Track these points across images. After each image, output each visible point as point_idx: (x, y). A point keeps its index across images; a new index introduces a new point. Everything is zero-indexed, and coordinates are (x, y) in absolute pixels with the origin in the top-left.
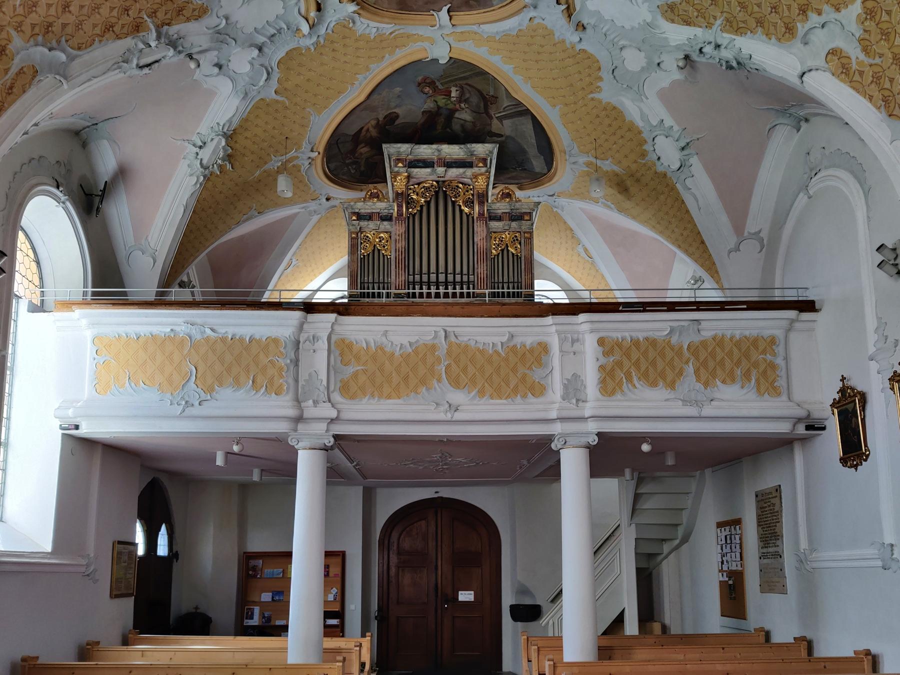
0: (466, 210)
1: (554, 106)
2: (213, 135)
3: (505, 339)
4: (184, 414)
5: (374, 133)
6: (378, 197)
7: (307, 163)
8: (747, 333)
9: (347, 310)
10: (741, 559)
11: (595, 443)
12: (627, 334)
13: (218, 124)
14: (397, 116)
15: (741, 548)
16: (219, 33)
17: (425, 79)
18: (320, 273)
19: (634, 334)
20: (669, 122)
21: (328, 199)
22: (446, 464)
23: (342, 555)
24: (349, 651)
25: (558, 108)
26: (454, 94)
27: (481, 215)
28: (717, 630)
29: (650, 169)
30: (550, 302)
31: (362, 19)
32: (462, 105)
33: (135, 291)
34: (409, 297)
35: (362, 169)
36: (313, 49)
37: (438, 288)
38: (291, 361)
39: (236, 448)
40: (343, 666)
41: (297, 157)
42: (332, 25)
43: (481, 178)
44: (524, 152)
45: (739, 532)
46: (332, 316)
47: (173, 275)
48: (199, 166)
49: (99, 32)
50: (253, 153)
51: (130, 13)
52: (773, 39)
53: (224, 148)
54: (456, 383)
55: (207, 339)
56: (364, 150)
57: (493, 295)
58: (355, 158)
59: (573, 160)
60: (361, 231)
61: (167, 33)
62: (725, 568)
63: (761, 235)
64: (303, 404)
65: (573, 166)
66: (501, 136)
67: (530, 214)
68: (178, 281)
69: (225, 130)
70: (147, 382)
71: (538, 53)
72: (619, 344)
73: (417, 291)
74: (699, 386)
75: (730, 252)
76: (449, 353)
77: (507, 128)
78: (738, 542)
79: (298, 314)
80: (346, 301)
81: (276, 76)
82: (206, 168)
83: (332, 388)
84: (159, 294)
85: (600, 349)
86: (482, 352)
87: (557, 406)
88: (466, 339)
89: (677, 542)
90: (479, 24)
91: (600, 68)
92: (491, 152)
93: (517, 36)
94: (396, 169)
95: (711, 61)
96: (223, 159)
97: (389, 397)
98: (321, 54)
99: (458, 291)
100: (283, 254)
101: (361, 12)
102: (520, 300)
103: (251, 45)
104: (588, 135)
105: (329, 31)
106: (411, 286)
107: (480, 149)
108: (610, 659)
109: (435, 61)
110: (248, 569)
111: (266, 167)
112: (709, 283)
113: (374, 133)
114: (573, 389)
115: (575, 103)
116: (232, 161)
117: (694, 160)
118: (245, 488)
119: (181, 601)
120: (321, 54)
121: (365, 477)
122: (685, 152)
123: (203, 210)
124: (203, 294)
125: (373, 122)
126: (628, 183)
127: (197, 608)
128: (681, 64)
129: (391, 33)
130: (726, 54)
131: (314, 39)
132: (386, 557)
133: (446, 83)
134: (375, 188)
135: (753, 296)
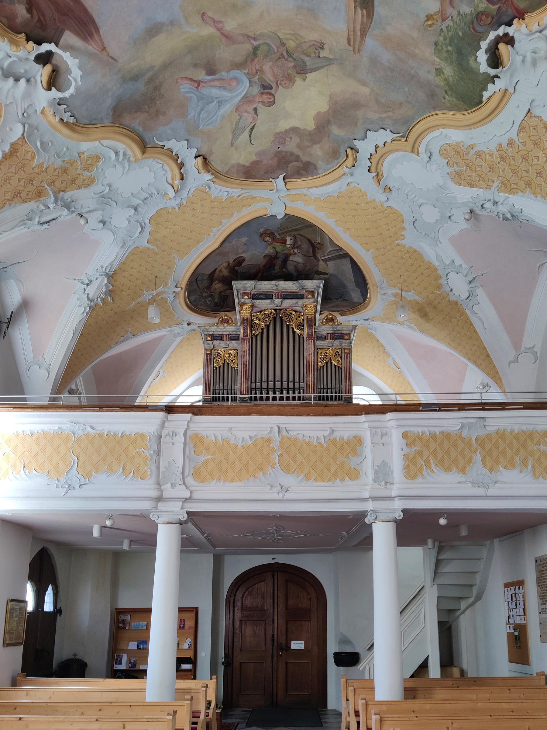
0: (298, 332)
1: (368, 250)
2: (97, 275)
3: (327, 433)
4: (67, 495)
5: (226, 273)
6: (228, 322)
7: (172, 296)
8: (524, 428)
9: (200, 411)
10: (524, 615)
11: (401, 518)
12: (426, 429)
13: (102, 266)
14: (244, 260)
15: (524, 605)
16: (103, 197)
17: (265, 232)
18: (182, 382)
19: (432, 429)
20: (459, 261)
21: (189, 324)
22: (280, 535)
23: (196, 611)
24: (197, 691)
25: (371, 252)
26: (289, 242)
27: (310, 335)
28: (506, 674)
29: (444, 298)
30: (367, 403)
31: (215, 185)
32: (295, 250)
33: (32, 397)
34: (251, 400)
35: (216, 300)
36: (177, 208)
37: (275, 393)
38: (154, 452)
39: (108, 523)
40: (191, 704)
41: (165, 292)
42: (192, 191)
43: (310, 307)
44: (344, 286)
45: (522, 591)
46: (188, 416)
47: (64, 382)
48: (86, 299)
49: (9, 198)
50: (129, 289)
51: (34, 183)
52: (539, 197)
53: (106, 285)
54: (287, 469)
55: (88, 435)
56: (217, 286)
57: (320, 398)
58: (210, 291)
59: (383, 292)
60: (214, 348)
61: (62, 198)
62: (511, 621)
63: (535, 349)
64: (163, 487)
65: (384, 297)
66: (326, 274)
67: (349, 334)
68: (68, 389)
69: (107, 271)
70: (38, 470)
71: (355, 210)
72: (419, 437)
73: (258, 395)
74: (486, 471)
75: (510, 363)
76: (281, 444)
77: (331, 267)
78: (522, 599)
79: (161, 415)
80: (201, 404)
81: (148, 228)
82: (92, 301)
83: (186, 473)
84: (51, 399)
85: (404, 441)
86: (308, 444)
87: (369, 487)
88: (295, 433)
89: (471, 600)
90: (308, 188)
91: (403, 221)
92: (318, 287)
93: (338, 197)
94: (243, 301)
95: (491, 214)
96: (105, 294)
97: (232, 480)
98: (184, 212)
99: (291, 395)
100: (153, 367)
101: (215, 180)
102: (341, 402)
103: (129, 206)
104: (395, 272)
105: (190, 195)
106: (253, 392)
107: (310, 284)
108: (414, 698)
109: (275, 216)
110: (118, 622)
111: (140, 299)
112: (494, 388)
113: (226, 273)
114: (382, 474)
115: (384, 248)
116: (112, 295)
117: (480, 291)
118: (117, 556)
119: (62, 651)
120: (184, 212)
121: (214, 546)
122: (473, 285)
123: (88, 333)
124: (88, 399)
125: (225, 264)
126: (428, 310)
127: (75, 655)
128: (467, 217)
129: (239, 196)
130: (503, 209)
131: (178, 201)
132: (232, 612)
133: (282, 233)
134: (226, 315)
135: (530, 398)
